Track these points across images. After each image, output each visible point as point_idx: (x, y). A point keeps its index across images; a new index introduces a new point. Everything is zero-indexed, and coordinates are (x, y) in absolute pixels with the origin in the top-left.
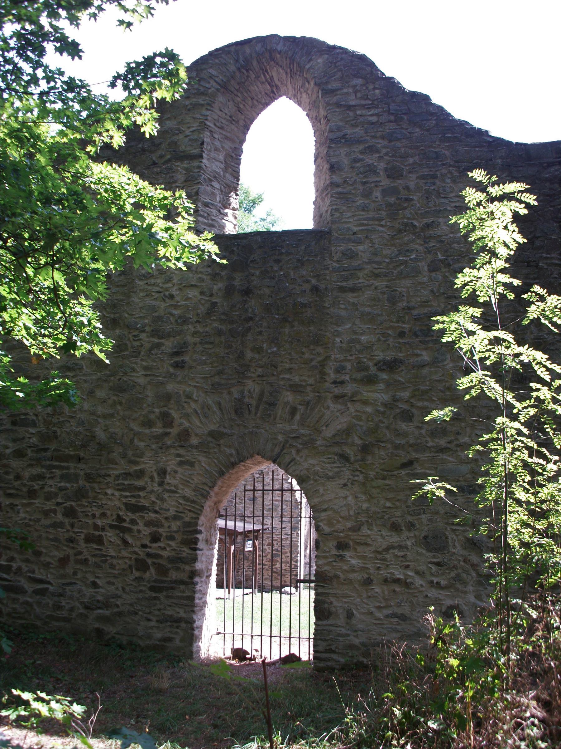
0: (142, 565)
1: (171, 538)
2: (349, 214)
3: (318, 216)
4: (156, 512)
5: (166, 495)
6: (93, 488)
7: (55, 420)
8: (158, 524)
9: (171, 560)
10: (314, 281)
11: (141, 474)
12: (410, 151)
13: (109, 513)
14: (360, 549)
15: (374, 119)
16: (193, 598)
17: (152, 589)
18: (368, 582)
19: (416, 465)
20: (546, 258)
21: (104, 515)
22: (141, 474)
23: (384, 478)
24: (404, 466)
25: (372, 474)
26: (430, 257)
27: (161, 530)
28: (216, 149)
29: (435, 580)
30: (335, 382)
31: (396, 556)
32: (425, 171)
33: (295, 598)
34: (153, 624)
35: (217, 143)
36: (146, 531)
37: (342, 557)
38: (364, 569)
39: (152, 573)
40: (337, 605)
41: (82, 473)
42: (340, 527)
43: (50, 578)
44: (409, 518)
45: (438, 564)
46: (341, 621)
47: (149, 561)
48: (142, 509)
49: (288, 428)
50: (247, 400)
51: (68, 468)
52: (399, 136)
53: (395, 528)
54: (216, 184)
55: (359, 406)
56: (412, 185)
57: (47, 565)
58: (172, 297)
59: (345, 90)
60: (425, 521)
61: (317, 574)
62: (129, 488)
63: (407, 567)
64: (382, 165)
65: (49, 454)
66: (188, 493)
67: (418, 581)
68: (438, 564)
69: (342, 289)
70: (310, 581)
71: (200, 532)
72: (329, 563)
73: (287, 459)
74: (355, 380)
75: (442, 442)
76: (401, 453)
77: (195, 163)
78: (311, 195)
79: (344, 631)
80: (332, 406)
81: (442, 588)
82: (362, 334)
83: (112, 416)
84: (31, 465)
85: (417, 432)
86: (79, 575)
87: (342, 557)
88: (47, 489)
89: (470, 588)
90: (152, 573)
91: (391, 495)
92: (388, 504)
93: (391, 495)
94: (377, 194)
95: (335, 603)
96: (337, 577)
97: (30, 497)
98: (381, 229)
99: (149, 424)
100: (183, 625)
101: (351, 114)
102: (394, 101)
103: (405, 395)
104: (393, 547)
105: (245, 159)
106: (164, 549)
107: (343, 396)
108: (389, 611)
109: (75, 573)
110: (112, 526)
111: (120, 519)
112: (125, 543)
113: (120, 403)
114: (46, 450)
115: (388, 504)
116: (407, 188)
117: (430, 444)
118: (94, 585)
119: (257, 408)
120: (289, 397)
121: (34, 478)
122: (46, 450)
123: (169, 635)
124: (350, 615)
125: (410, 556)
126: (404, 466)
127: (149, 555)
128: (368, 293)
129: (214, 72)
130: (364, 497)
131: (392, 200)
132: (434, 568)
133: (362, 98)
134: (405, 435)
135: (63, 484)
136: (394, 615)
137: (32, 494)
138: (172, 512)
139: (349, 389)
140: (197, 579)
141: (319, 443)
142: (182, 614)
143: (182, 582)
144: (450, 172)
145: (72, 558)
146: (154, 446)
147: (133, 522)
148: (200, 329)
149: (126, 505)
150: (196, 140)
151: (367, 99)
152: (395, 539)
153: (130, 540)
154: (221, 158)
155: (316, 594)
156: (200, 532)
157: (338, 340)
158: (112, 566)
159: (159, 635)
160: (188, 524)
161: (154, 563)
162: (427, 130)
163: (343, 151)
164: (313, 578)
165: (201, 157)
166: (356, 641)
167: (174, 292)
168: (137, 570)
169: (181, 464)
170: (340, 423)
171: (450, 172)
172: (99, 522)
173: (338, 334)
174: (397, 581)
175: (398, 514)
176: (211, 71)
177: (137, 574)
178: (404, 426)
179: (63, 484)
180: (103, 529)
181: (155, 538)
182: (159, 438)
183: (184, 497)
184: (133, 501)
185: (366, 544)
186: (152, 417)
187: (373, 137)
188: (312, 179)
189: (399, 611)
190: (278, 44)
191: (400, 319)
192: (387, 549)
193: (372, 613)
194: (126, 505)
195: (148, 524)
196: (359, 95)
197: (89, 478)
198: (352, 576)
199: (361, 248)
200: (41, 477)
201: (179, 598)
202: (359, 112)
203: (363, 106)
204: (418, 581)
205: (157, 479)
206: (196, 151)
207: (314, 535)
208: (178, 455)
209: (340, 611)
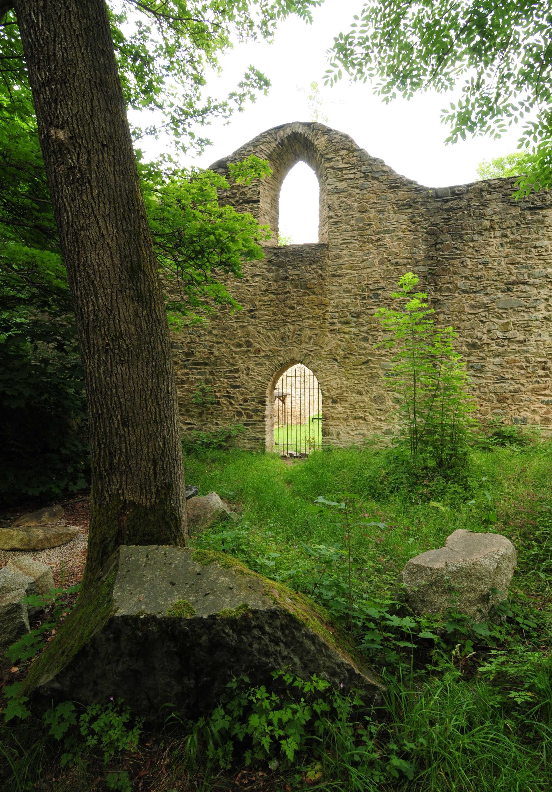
0: (239, 414)
1: (253, 400)
2: (338, 234)
3: (321, 235)
4: (245, 388)
5: (250, 381)
6: (214, 378)
7: (192, 346)
8: (247, 394)
9: (253, 411)
10: (320, 272)
11: (237, 371)
12: (372, 195)
13: (222, 390)
14: (343, 403)
15: (352, 176)
16: (264, 428)
17: (245, 424)
18: (346, 420)
19: (370, 362)
20: (442, 255)
21: (220, 391)
22: (237, 371)
23: (354, 369)
24: (364, 363)
25: (348, 368)
26: (380, 257)
27: (248, 397)
28: (266, 196)
29: (379, 417)
30: (330, 323)
31: (360, 406)
32: (380, 208)
33: (316, 413)
34: (246, 441)
35: (266, 192)
36: (241, 398)
37: (334, 408)
38: (345, 412)
39: (244, 418)
40: (333, 430)
41: (207, 371)
42: (333, 393)
43: (195, 422)
44: (366, 388)
45: (380, 410)
46: (335, 437)
47: (243, 412)
48: (238, 387)
49: (308, 346)
50: (287, 333)
51: (200, 369)
52: (366, 186)
53: (360, 393)
54: (266, 217)
55: (343, 335)
56: (372, 216)
57: (193, 417)
58: (248, 281)
59: (337, 158)
60: (374, 389)
61: (323, 415)
62: (232, 377)
63: (365, 411)
64: (356, 205)
65: (190, 362)
66: (260, 378)
67: (371, 418)
68: (380, 410)
69: (334, 276)
70: (319, 419)
71: (267, 397)
72: (328, 410)
73: (308, 361)
74: (340, 322)
75: (383, 352)
76: (363, 357)
77: (256, 205)
78: (316, 222)
79: (336, 441)
80: (328, 335)
81: (382, 421)
82: (344, 298)
83: (221, 343)
84: (182, 368)
85: (370, 347)
86: (209, 420)
87: (334, 408)
88: (190, 379)
89: (395, 421)
90: (244, 418)
91: (357, 377)
92: (356, 382)
93: (357, 377)
94: (353, 222)
95: (332, 428)
96: (332, 417)
97: (182, 384)
98: (355, 241)
99: (240, 346)
100: (260, 441)
101: (340, 173)
102: (364, 165)
103: (365, 329)
104: (359, 402)
105: (281, 200)
106: (250, 406)
107: (334, 330)
108: (356, 432)
109: (207, 419)
110: (224, 396)
111: (228, 392)
112: (231, 404)
113: (225, 336)
114: (188, 360)
115: (356, 382)
116: (369, 218)
117: (377, 353)
118: (217, 424)
119: (293, 336)
120: (308, 332)
121: (184, 374)
122: (188, 360)
123: (253, 446)
124: (338, 434)
125: (367, 407)
126: (364, 363)
127: (243, 409)
128: (348, 277)
129: (263, 147)
130: (344, 379)
131: (361, 225)
132: (378, 412)
133: (346, 163)
134: (365, 349)
135: (198, 377)
136: (360, 434)
137: (183, 382)
138: (253, 388)
139: (338, 326)
140: (266, 419)
141: (323, 353)
142: (260, 436)
143: (260, 421)
144: (393, 208)
145: (205, 412)
146: (243, 357)
147: (234, 393)
148: (263, 298)
149: (231, 385)
150: (255, 191)
151: (349, 163)
152: (359, 398)
153: (233, 402)
154: (269, 201)
155: (323, 425)
156: (267, 397)
157: (332, 302)
158: (225, 415)
159: (249, 446)
160: (261, 394)
161: (245, 413)
162: (382, 182)
163: (335, 197)
164: (320, 417)
165: (258, 201)
166: (342, 446)
167: (248, 278)
168: (237, 416)
169: (256, 364)
170: (333, 344)
171: (393, 208)
172: (217, 394)
173: (332, 299)
174: (361, 418)
175: (361, 386)
176: (261, 146)
177: (237, 418)
178: (364, 344)
179: (198, 377)
180: (220, 398)
181: (246, 401)
182: (245, 352)
183: (259, 381)
184: (234, 384)
185: (346, 401)
186: (241, 342)
187: (352, 187)
188: (317, 213)
189: (362, 432)
190: (299, 128)
191: (364, 290)
192: (356, 403)
193: (348, 433)
194: (231, 385)
195: (242, 394)
196: (345, 161)
197: (211, 373)
198: (339, 416)
199: (344, 252)
200: (187, 374)
201: (257, 428)
202: (344, 172)
203: (346, 168)
204: (371, 418)
205: (245, 372)
206: (255, 198)
207: (321, 397)
208: (255, 361)
209: (334, 432)
